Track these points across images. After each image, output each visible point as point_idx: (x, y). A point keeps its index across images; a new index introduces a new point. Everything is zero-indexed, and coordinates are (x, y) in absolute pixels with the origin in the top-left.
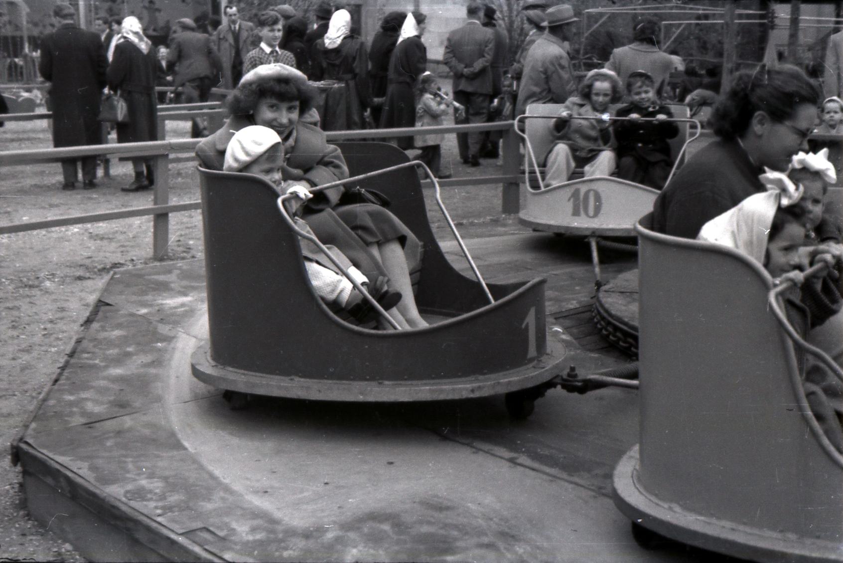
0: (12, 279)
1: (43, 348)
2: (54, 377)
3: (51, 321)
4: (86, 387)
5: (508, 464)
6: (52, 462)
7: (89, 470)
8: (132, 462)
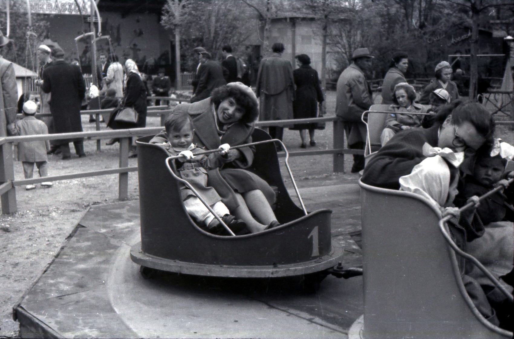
0: (33, 211)
1: (46, 252)
2: (45, 269)
3: (53, 236)
4: (62, 275)
5: (308, 322)
6: (35, 319)
7: (55, 324)
8: (82, 319)
